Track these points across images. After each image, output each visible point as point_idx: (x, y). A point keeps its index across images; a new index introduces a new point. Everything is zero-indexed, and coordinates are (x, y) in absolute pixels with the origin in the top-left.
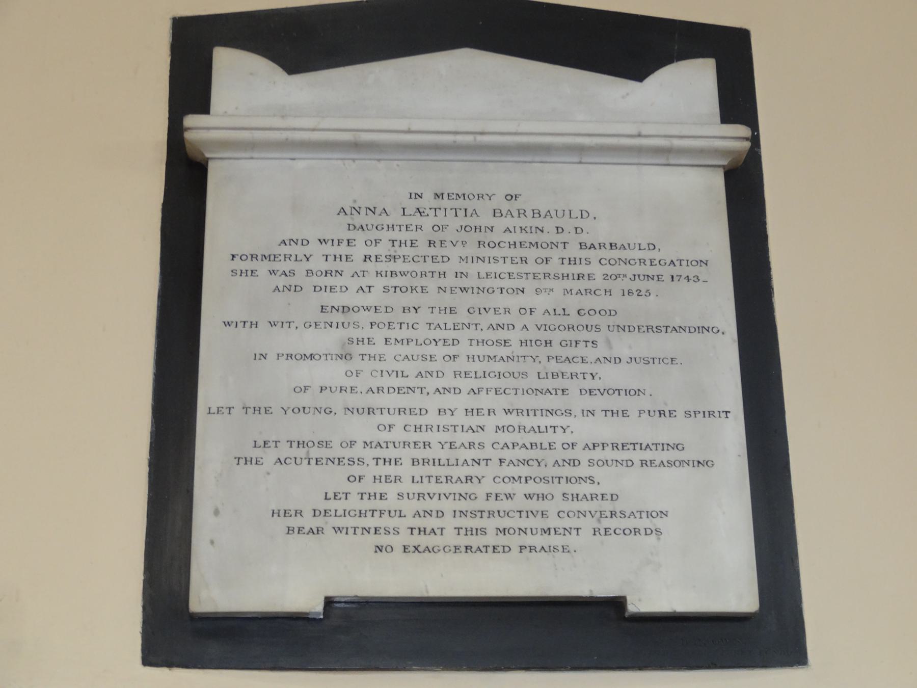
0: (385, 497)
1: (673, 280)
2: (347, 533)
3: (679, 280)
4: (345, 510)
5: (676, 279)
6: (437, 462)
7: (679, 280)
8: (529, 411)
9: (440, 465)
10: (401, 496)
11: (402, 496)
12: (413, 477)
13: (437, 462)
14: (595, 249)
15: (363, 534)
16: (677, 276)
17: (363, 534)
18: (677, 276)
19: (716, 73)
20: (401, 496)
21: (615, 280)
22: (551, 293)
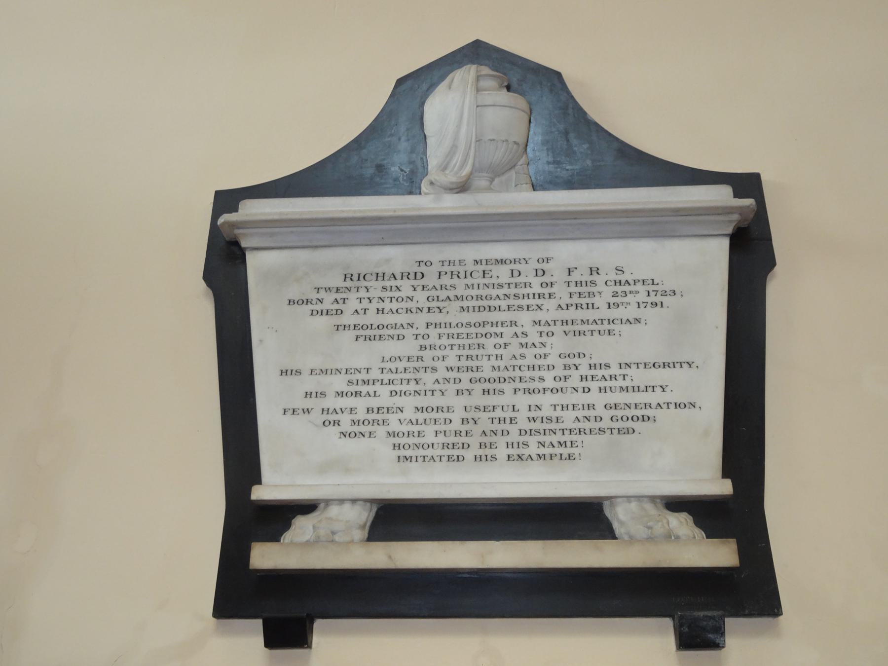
0: (374, 435)
1: (639, 307)
2: (411, 461)
3: (656, 295)
4: (389, 380)
5: (642, 306)
6: (636, 389)
7: (656, 295)
8: (403, 380)
9: (438, 301)
10: (549, 419)
11: (527, 445)
12: (417, 420)
13: (636, 389)
14: (629, 285)
15: (544, 442)
16: (643, 303)
17: (544, 442)
18: (643, 303)
19: (655, 567)
20: (549, 419)
21: (588, 392)
22: (628, 306)
